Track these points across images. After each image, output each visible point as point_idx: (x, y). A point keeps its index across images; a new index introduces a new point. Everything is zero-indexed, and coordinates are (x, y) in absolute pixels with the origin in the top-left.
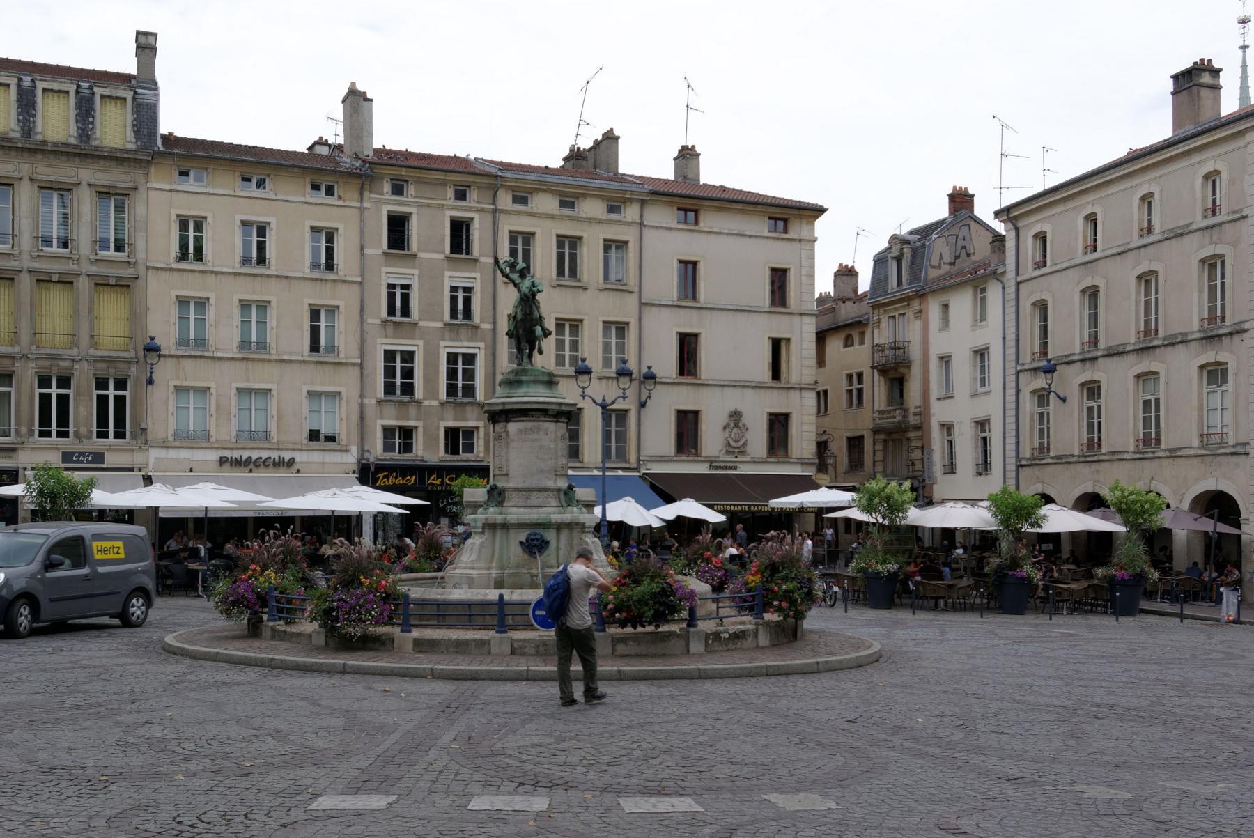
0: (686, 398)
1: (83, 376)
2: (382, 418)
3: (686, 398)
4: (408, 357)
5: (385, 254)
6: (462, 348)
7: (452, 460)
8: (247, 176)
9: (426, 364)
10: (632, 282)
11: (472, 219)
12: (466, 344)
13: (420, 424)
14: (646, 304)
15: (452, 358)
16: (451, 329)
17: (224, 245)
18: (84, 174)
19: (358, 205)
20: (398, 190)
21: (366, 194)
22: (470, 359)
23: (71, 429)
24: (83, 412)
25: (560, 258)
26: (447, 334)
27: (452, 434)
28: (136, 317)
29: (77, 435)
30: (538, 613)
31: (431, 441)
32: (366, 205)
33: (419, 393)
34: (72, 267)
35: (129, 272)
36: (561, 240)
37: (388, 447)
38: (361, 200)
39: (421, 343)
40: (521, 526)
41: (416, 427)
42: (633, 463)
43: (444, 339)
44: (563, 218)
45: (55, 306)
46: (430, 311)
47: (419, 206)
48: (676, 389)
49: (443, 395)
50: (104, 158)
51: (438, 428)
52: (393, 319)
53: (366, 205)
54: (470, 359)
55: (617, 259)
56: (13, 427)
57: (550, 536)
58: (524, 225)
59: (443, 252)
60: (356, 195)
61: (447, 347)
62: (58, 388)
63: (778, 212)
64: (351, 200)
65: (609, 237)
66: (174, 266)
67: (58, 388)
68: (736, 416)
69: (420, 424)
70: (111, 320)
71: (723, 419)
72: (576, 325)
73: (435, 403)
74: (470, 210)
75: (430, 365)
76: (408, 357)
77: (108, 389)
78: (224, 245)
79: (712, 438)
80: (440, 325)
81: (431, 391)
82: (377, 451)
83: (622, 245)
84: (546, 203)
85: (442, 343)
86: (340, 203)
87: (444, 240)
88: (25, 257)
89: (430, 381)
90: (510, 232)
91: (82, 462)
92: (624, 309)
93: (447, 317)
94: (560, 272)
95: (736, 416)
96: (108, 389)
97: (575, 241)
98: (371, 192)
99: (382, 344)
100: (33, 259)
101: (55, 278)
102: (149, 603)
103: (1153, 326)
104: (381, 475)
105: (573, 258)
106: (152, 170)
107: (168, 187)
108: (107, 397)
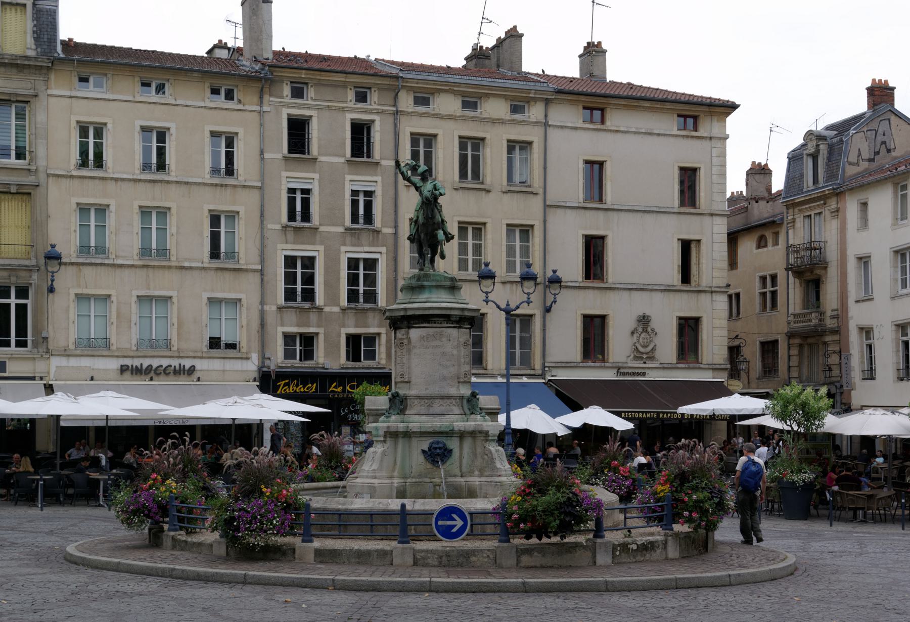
2: (282, 325)
6: (363, 252)
8: (84, 75)
12: (367, 249)
13: (321, 330)
14: (551, 206)
15: (353, 264)
17: (124, 151)
19: (258, 108)
22: (371, 264)
26: (348, 239)
30: (440, 523)
31: (331, 348)
32: (265, 108)
33: (320, 299)
36: (463, 141)
38: (261, 104)
40: (423, 434)
43: (345, 244)
44: (465, 119)
46: (331, 218)
49: (344, 301)
51: (339, 335)
53: (265, 108)
54: (371, 264)
57: (453, 444)
58: (425, 126)
60: (256, 99)
61: (348, 251)
64: (251, 104)
68: (644, 321)
69: (321, 330)
71: (631, 324)
76: (309, 262)
77: (9, 297)
78: (124, 151)
79: (619, 344)
80: (341, 229)
81: (332, 299)
82: (278, 359)
83: (526, 145)
85: (343, 249)
86: (240, 107)
92: (528, 211)
94: (463, 175)
95: (644, 321)
96: (9, 297)
97: (478, 143)
98: (270, 95)
99: (282, 250)
104: (283, 383)
105: (476, 160)
106: (52, 76)
107: (68, 93)
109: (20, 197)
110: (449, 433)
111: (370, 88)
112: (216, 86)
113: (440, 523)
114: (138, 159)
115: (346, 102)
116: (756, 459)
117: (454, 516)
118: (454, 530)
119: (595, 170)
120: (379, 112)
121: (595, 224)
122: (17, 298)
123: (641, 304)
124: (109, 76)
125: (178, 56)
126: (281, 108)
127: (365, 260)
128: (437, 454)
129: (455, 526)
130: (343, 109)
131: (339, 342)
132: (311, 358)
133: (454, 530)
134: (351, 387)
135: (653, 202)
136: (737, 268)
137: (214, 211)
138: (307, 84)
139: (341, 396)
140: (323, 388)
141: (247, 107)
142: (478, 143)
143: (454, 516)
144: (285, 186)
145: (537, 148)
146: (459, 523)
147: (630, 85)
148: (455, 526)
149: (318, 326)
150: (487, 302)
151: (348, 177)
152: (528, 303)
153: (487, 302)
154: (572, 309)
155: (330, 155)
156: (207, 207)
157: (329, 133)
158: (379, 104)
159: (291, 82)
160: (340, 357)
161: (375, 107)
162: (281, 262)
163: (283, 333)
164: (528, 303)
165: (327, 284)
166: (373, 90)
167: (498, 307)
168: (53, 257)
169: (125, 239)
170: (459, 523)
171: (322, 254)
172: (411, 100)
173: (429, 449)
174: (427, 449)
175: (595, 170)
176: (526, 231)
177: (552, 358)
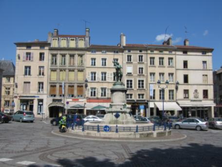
0: (186, 87)
1: (76, 85)
3: (186, 87)
4: (131, 81)
6: (141, 79)
7: (139, 99)
9: (134, 82)
10: (174, 66)
14: (178, 69)
15: (139, 81)
17: (99, 63)
18: (77, 52)
20: (129, 51)
22: (143, 81)
25: (160, 62)
27: (139, 95)
28: (85, 76)
31: (135, 97)
33: (145, 88)
34: (57, 68)
35: (83, 68)
36: (160, 58)
37: (139, 98)
40: (114, 112)
42: (175, 100)
44: (169, 54)
45: (72, 74)
48: (183, 86)
49: (138, 88)
54: (143, 81)
57: (120, 114)
58: (152, 56)
61: (138, 79)
63: (203, 51)
65: (26, 65)
68: (196, 91)
70: (80, 75)
71: (194, 91)
75: (135, 83)
76: (131, 81)
78: (99, 63)
79: (191, 95)
81: (135, 87)
83: (172, 59)
89: (135, 85)
92: (172, 70)
93: (138, 74)
94: (160, 64)
95: (196, 91)
97: (163, 58)
100: (60, 66)
102: (56, 125)
103: (116, 77)
105: (162, 61)
114: (91, 63)
116: (170, 115)
119: (185, 64)
121: (186, 72)
123: (195, 87)
126: (126, 54)
128: (117, 116)
135: (199, 68)
136: (43, 60)
142: (163, 58)
144: (138, 67)
145: (174, 59)
146: (108, 129)
147: (193, 47)
154: (182, 88)
156: (45, 66)
162: (126, 81)
168: (86, 81)
169: (99, 76)
170: (108, 129)
175: (185, 64)
176: (172, 74)
177: (177, 99)
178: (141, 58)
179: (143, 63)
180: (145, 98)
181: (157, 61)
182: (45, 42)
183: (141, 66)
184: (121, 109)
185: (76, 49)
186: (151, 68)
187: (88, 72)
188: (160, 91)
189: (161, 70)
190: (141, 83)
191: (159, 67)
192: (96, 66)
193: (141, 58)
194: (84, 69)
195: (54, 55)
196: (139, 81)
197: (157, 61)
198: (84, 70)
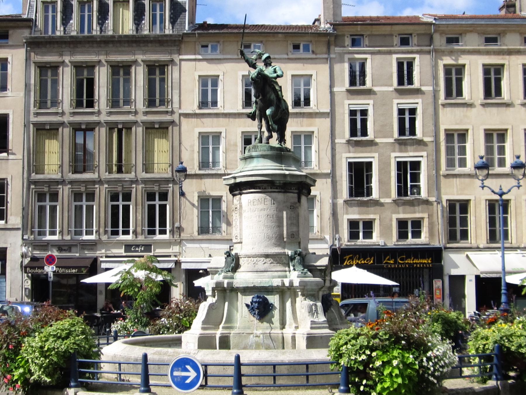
2: (347, 214)
5: (348, 91)
8: (204, 44)
9: (380, 170)
11: (414, 59)
12: (411, 154)
13: (377, 217)
16: (401, 144)
19: (326, 56)
21: (332, 48)
22: (416, 165)
23: (131, 229)
24: (137, 216)
26: (397, 146)
27: (353, 224)
28: (175, 151)
29: (135, 232)
30: (176, 373)
31: (385, 231)
32: (332, 56)
36: (487, 70)
38: (329, 52)
39: (376, 155)
41: (423, 218)
43: (394, 151)
44: (488, 53)
46: (382, 132)
47: (372, 53)
49: (394, 194)
50: (151, 42)
51: (391, 220)
52: (355, 139)
53: (332, 56)
55: (124, 79)
56: (95, 229)
59: (392, 85)
60: (325, 49)
61: (397, 156)
62: (160, 200)
64: (322, 53)
66: (198, 111)
67: (160, 200)
69: (377, 217)
72: (463, 135)
73: (389, 200)
74: (412, 52)
77: (118, 201)
80: (391, 140)
82: (344, 239)
84: (472, 41)
85: (393, 155)
86: (314, 56)
87: (392, 76)
88: (67, 114)
90: (484, 65)
91: (137, 251)
93: (396, 135)
96: (118, 201)
97: (499, 69)
98: (336, 46)
99: (346, 156)
101: (157, 126)
104: (348, 257)
106: (183, 46)
107: (193, 57)
108: (154, 206)
109: (161, 130)
110: (270, 290)
111: (411, 34)
112: (297, 42)
113: (176, 373)
115: (393, 46)
117: (188, 367)
118: (188, 381)
120: (417, 52)
122: (123, 201)
124: (221, 42)
125: (296, 27)
127: (411, 162)
129: (188, 377)
130: (390, 53)
131: (391, 225)
132: (371, 237)
133: (188, 381)
134: (401, 260)
137: (296, 132)
138: (363, 35)
139: (393, 266)
140: (380, 261)
141: (318, 56)
143: (188, 367)
146: (192, 374)
148: (188, 377)
149: (375, 214)
150: (483, 187)
151: (396, 101)
152: (519, 187)
153: (483, 187)
155: (381, 86)
156: (10, 112)
157: (382, 68)
158: (418, 46)
159: (351, 35)
160: (392, 236)
161: (415, 48)
163: (348, 219)
164: (519, 187)
165: (380, 182)
166: (413, 35)
167: (493, 191)
171: (377, 159)
172: (444, 41)
173: (252, 303)
174: (250, 304)
178: (405, 73)
179: (372, 143)
180: (424, 239)
181: (473, 85)
182: (16, 16)
183: (407, 102)
184: (348, 335)
185: (135, 42)
186: (448, 109)
187: (190, 133)
188: (492, 206)
189: (495, 118)
190: (408, 172)
191: (484, 105)
192: (220, 109)
193: (405, 73)
194: (172, 123)
195: (47, 71)
196: (401, 166)
197: (473, 85)
198: (173, 131)
